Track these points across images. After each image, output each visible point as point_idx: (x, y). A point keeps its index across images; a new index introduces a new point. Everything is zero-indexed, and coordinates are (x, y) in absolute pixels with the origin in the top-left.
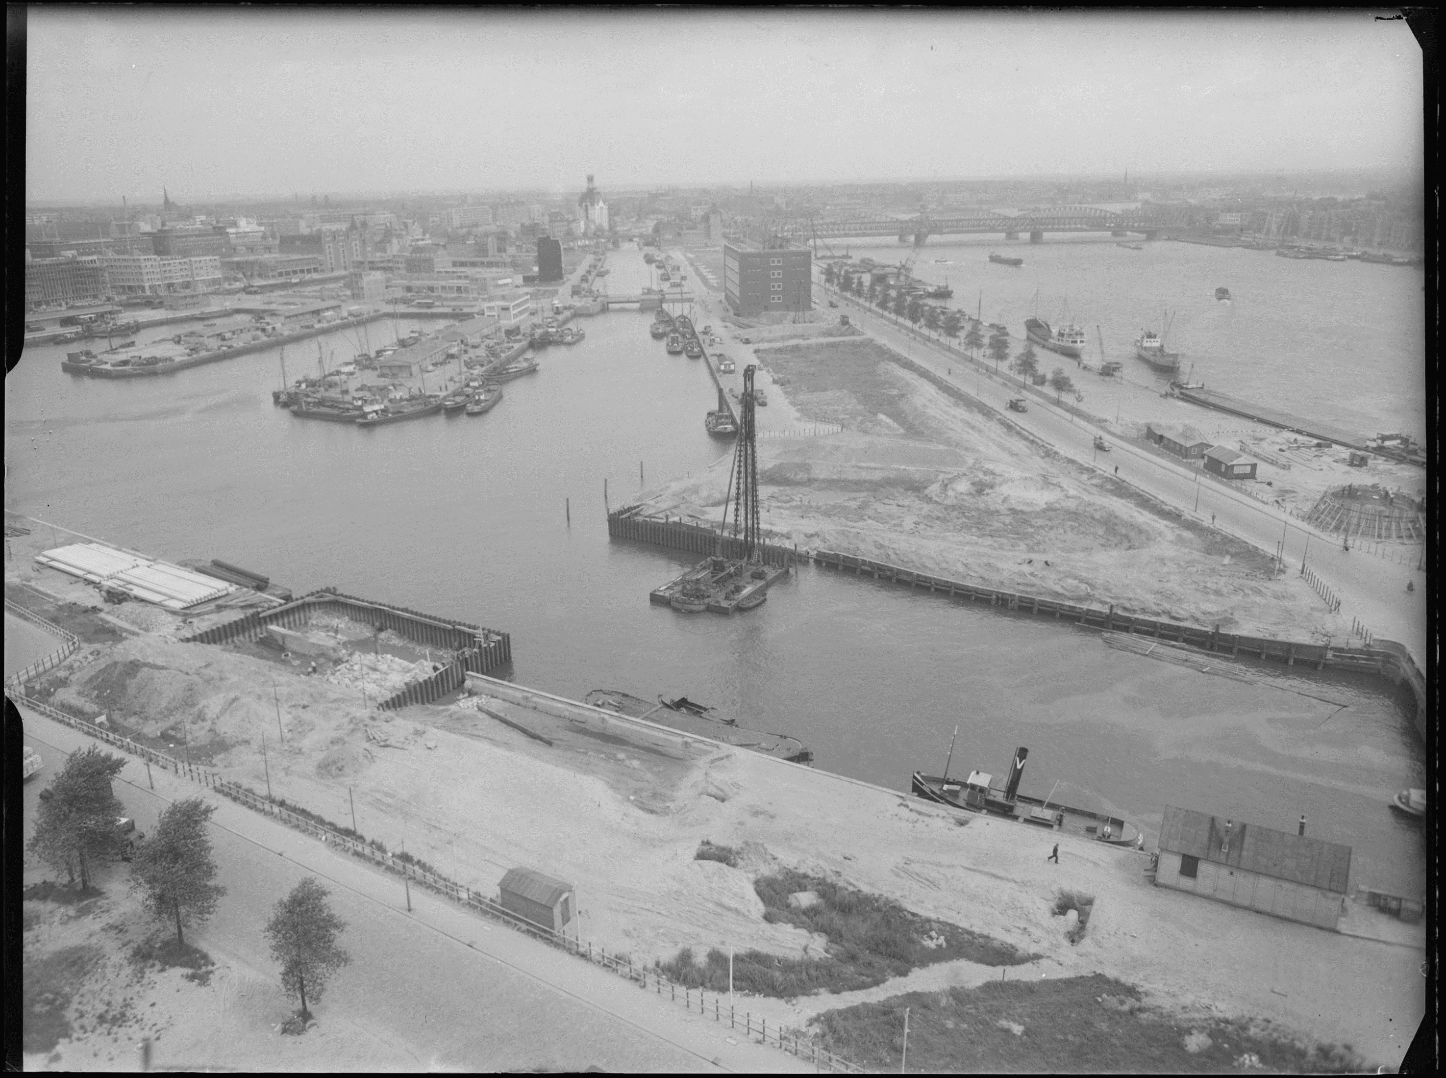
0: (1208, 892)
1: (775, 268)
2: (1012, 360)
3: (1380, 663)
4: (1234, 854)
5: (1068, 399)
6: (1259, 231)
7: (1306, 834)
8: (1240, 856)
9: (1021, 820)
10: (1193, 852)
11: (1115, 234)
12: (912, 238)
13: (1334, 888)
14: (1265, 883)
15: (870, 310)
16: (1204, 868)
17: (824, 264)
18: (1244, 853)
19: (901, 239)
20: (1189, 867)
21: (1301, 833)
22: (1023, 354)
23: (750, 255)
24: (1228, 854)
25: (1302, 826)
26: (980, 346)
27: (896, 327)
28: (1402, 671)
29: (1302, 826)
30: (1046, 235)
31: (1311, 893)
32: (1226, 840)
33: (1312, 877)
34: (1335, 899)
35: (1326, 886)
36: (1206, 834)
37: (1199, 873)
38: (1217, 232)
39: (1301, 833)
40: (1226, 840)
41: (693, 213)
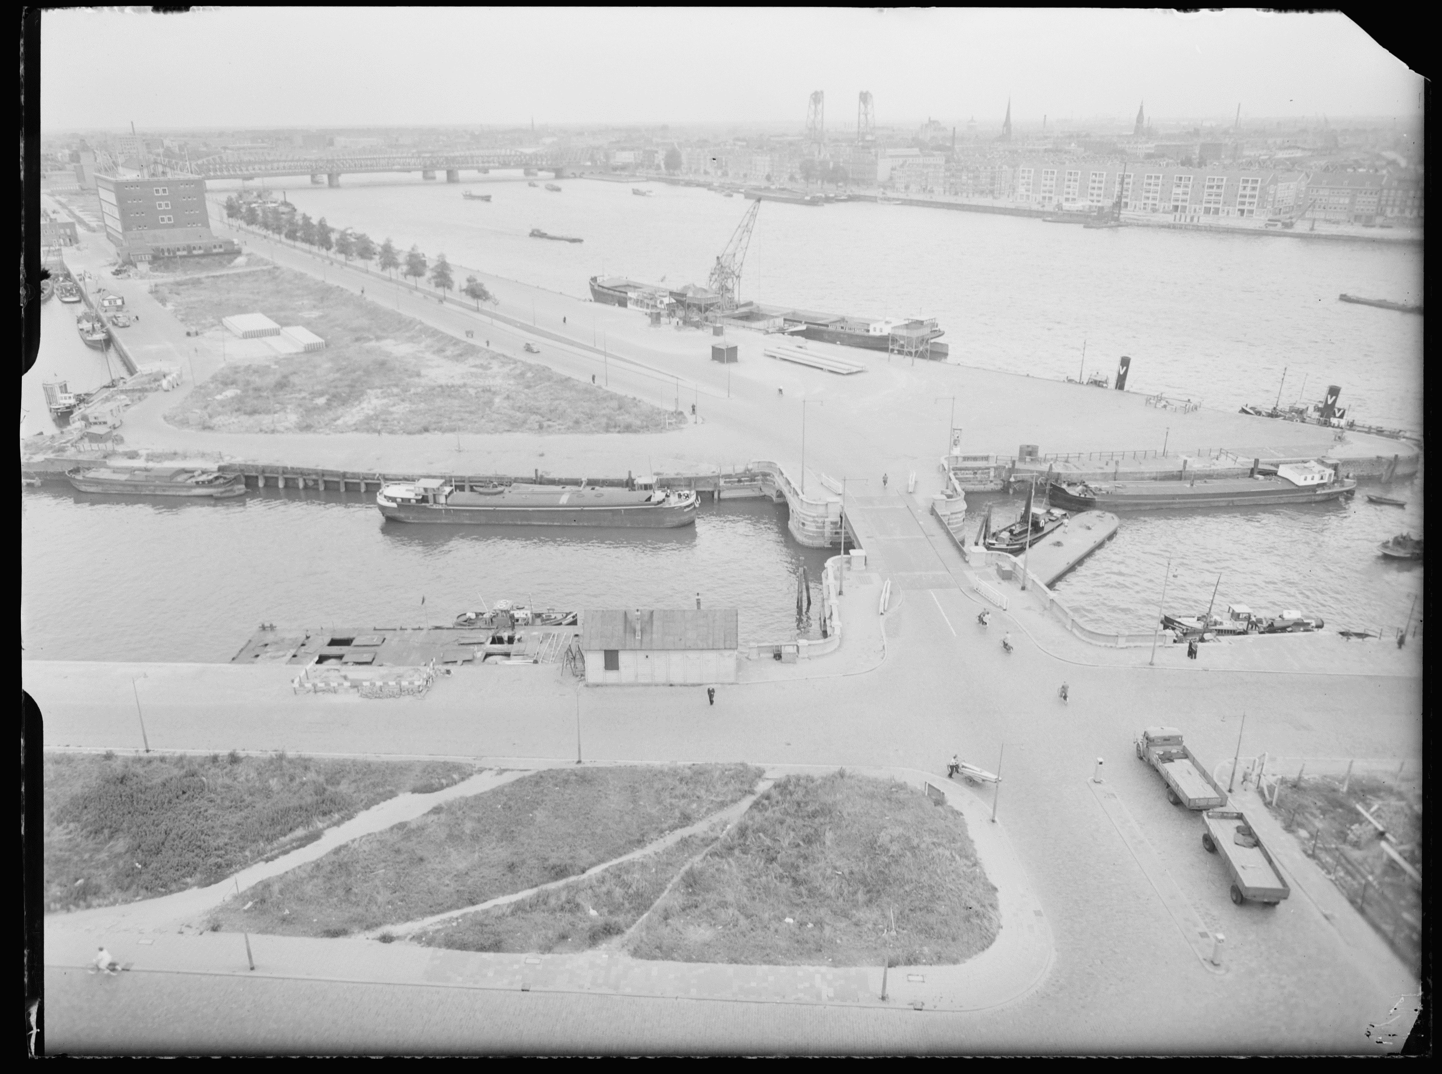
0: (631, 679)
1: (162, 198)
2: (429, 274)
3: (760, 482)
4: (646, 639)
5: (485, 306)
6: (650, 167)
7: (702, 607)
8: (651, 640)
9: (459, 662)
10: (612, 647)
11: (527, 173)
12: (325, 178)
13: (728, 647)
14: (676, 657)
15: (280, 242)
16: (624, 658)
17: (223, 198)
18: (655, 636)
19: (314, 181)
20: (611, 660)
21: (699, 608)
22: (437, 266)
23: (127, 184)
24: (641, 641)
25: (699, 602)
26: (396, 265)
27: (310, 256)
28: (776, 484)
29: (699, 602)
30: (462, 174)
31: (711, 655)
32: (638, 627)
33: (710, 642)
34: (729, 656)
35: (722, 647)
36: (621, 628)
37: (621, 665)
38: (615, 169)
39: (699, 608)
40: (638, 627)
41: (59, 155)
